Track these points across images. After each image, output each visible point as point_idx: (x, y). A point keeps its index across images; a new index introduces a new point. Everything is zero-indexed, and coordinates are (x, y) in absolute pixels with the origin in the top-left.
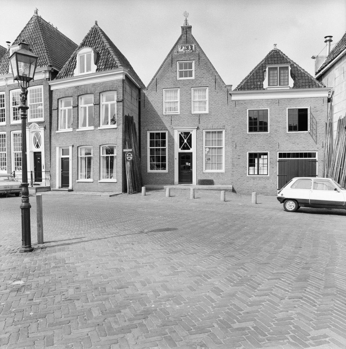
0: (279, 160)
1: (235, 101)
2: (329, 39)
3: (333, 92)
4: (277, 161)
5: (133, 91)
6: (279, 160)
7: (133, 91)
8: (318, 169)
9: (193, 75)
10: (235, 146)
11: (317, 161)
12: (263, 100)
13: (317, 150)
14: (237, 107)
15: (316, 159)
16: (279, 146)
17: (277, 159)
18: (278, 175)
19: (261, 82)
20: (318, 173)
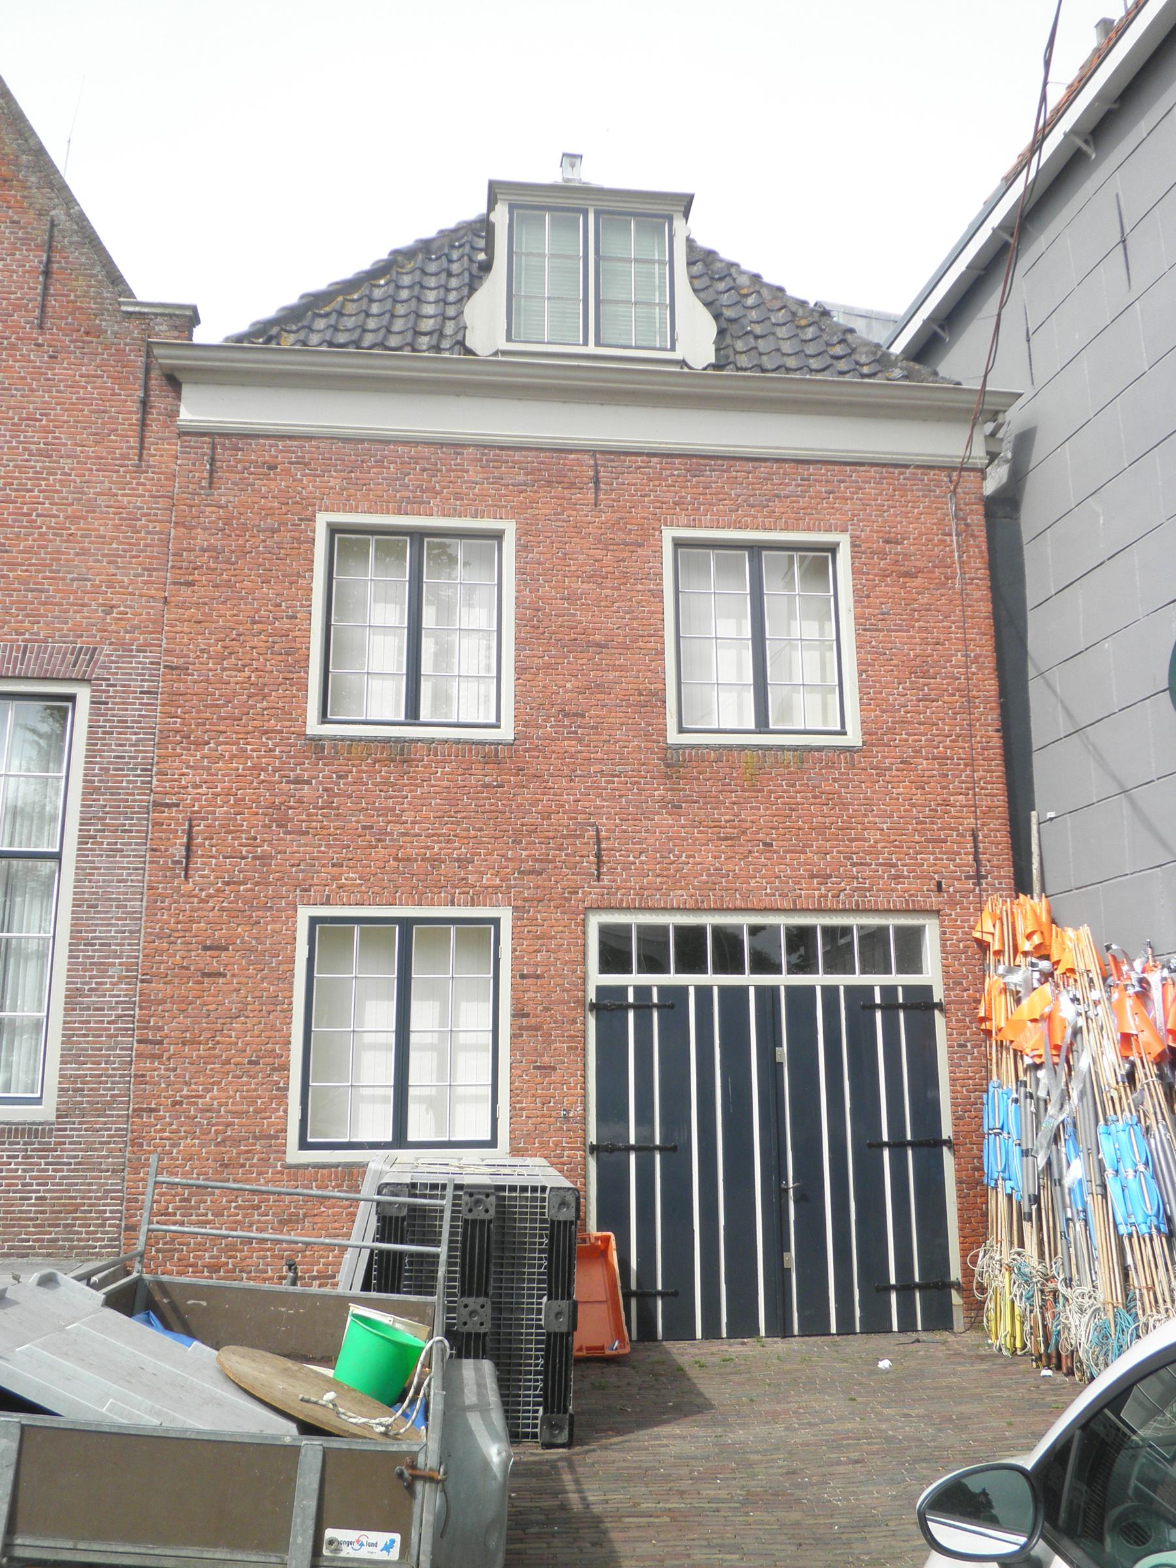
0: (601, 990)
1: (216, 437)
2: (572, 158)
3: (1025, 441)
4: (581, 1002)
5: (1031, 468)
6: (601, 990)
7: (1031, 468)
8: (953, 1080)
9: (101, 1561)
10: (179, 851)
11: (939, 1006)
12: (457, 446)
13: (934, 901)
14: (225, 494)
15: (928, 990)
16: (599, 856)
17: (584, 979)
18: (594, 1149)
19: (744, 291)
20: (957, 1118)
